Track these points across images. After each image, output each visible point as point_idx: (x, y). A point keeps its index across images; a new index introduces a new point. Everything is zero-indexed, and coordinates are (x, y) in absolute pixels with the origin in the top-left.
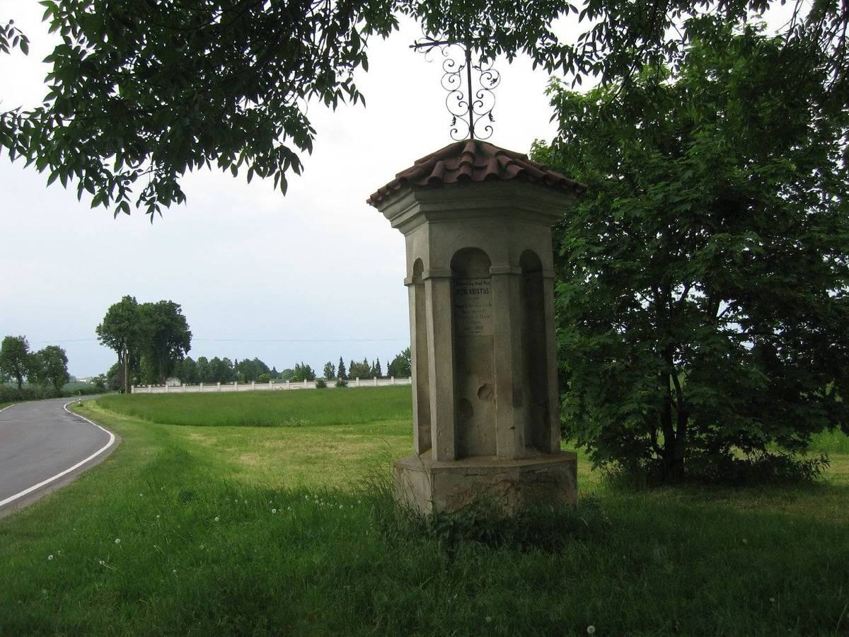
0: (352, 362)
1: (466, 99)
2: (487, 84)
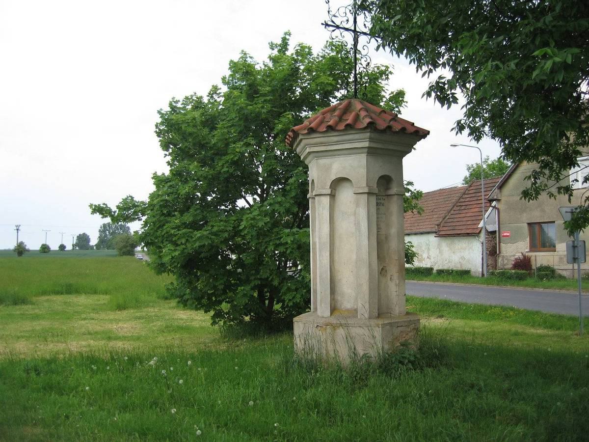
0: (478, 143)
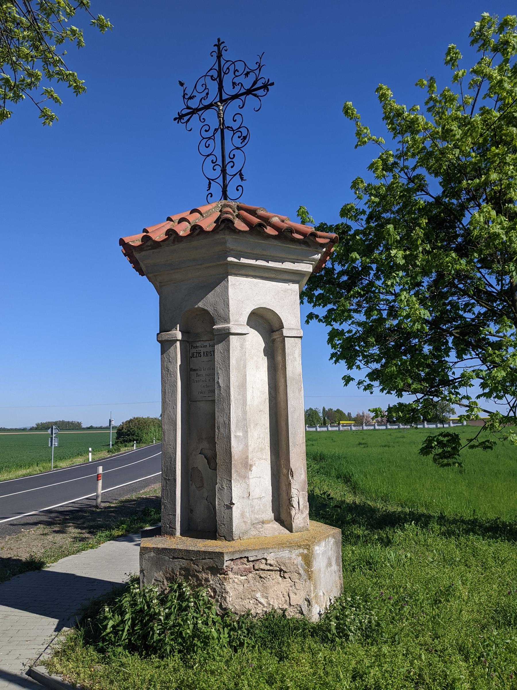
1: (220, 162)
2: (238, 142)
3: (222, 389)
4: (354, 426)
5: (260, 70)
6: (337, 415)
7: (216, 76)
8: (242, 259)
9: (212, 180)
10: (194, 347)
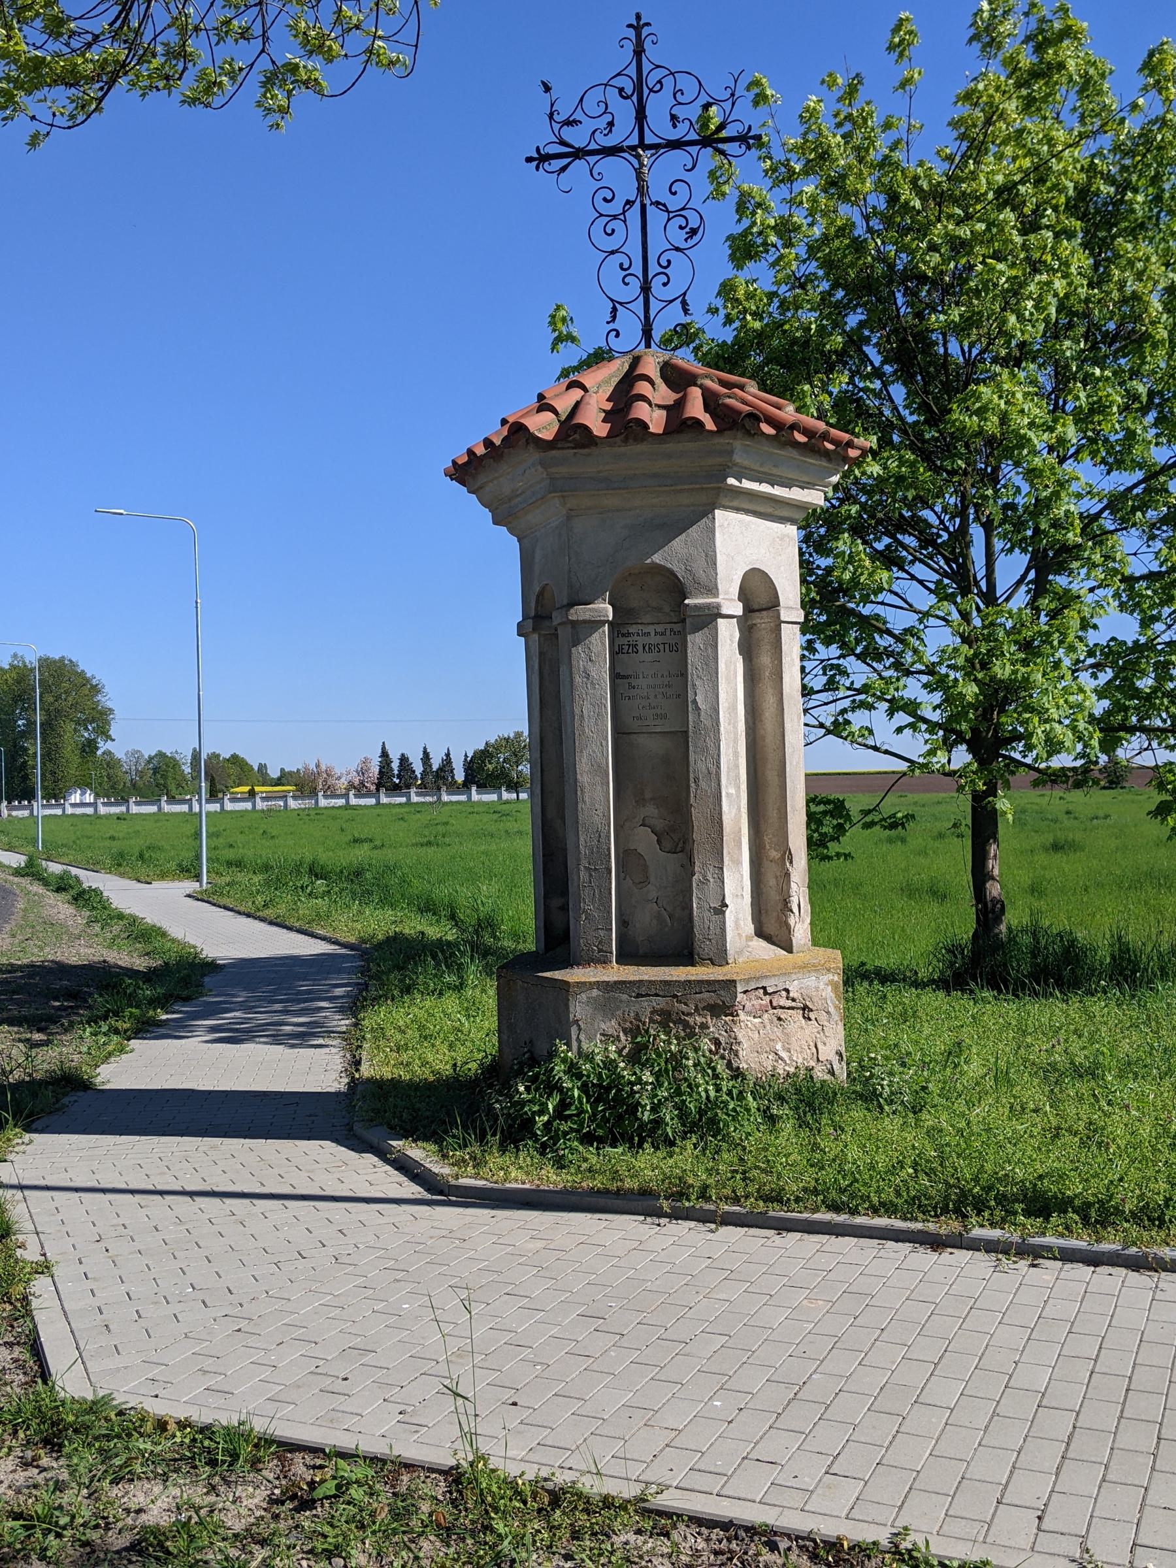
1: (637, 269)
2: (679, 237)
3: (702, 713)
4: (295, 798)
5: (733, 104)
6: (233, 770)
7: (629, 90)
8: (744, 480)
9: (621, 304)
10: (623, 635)
